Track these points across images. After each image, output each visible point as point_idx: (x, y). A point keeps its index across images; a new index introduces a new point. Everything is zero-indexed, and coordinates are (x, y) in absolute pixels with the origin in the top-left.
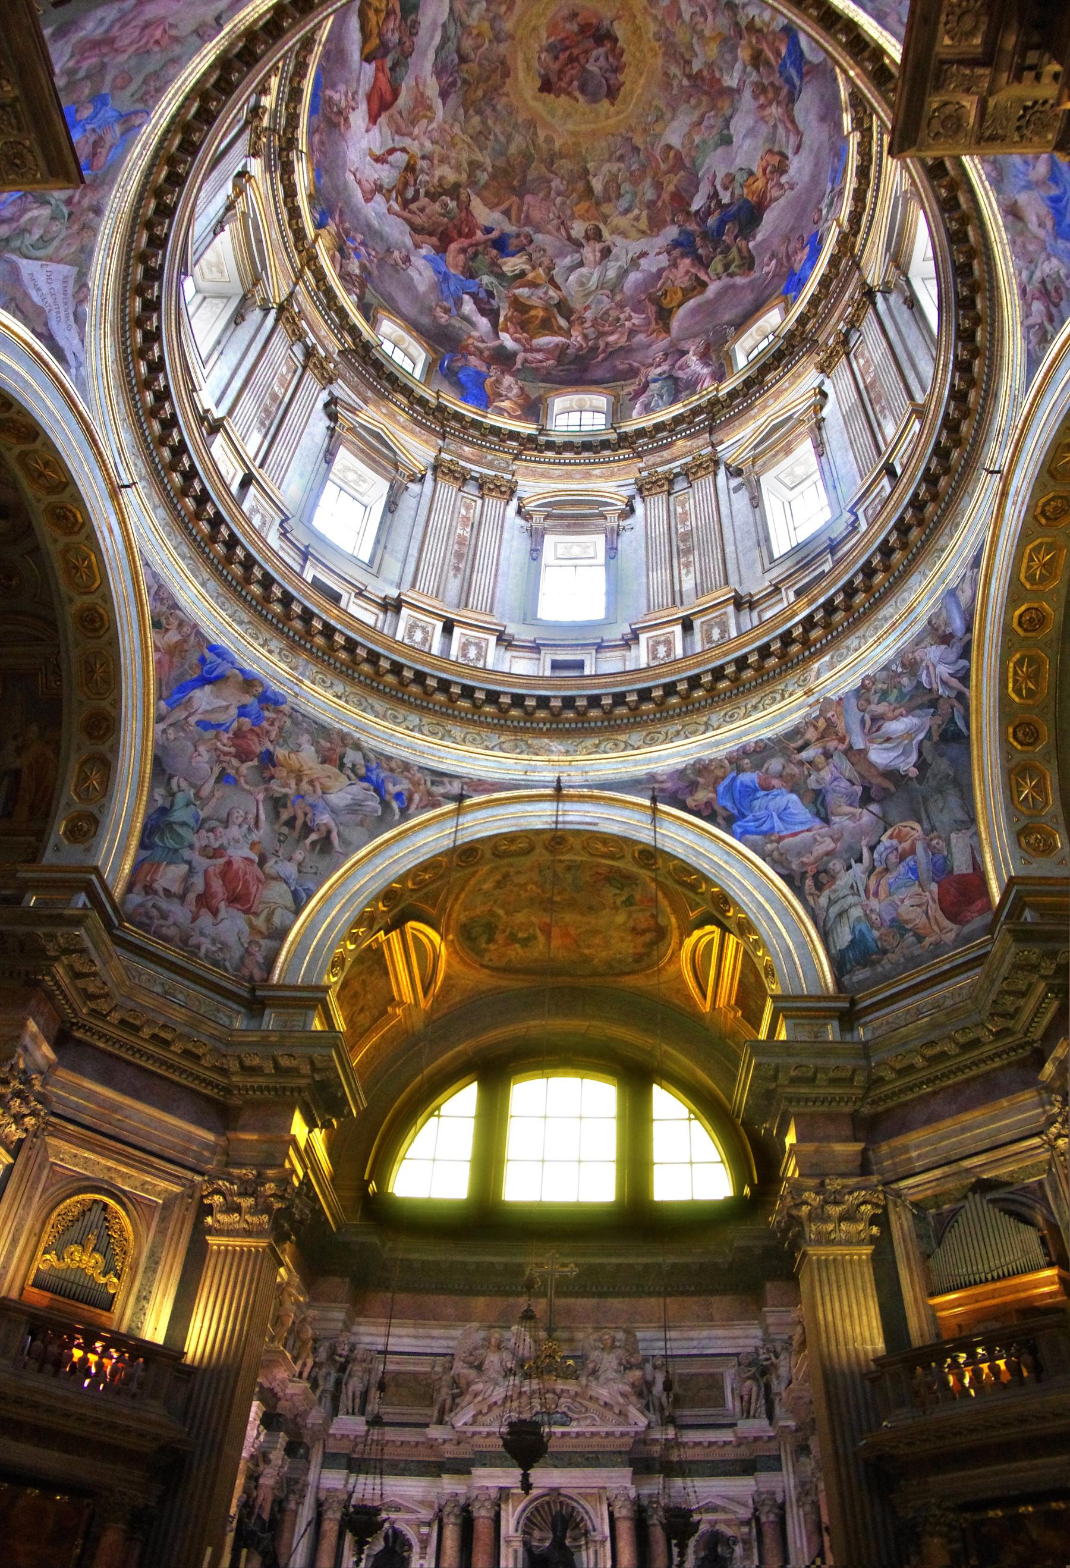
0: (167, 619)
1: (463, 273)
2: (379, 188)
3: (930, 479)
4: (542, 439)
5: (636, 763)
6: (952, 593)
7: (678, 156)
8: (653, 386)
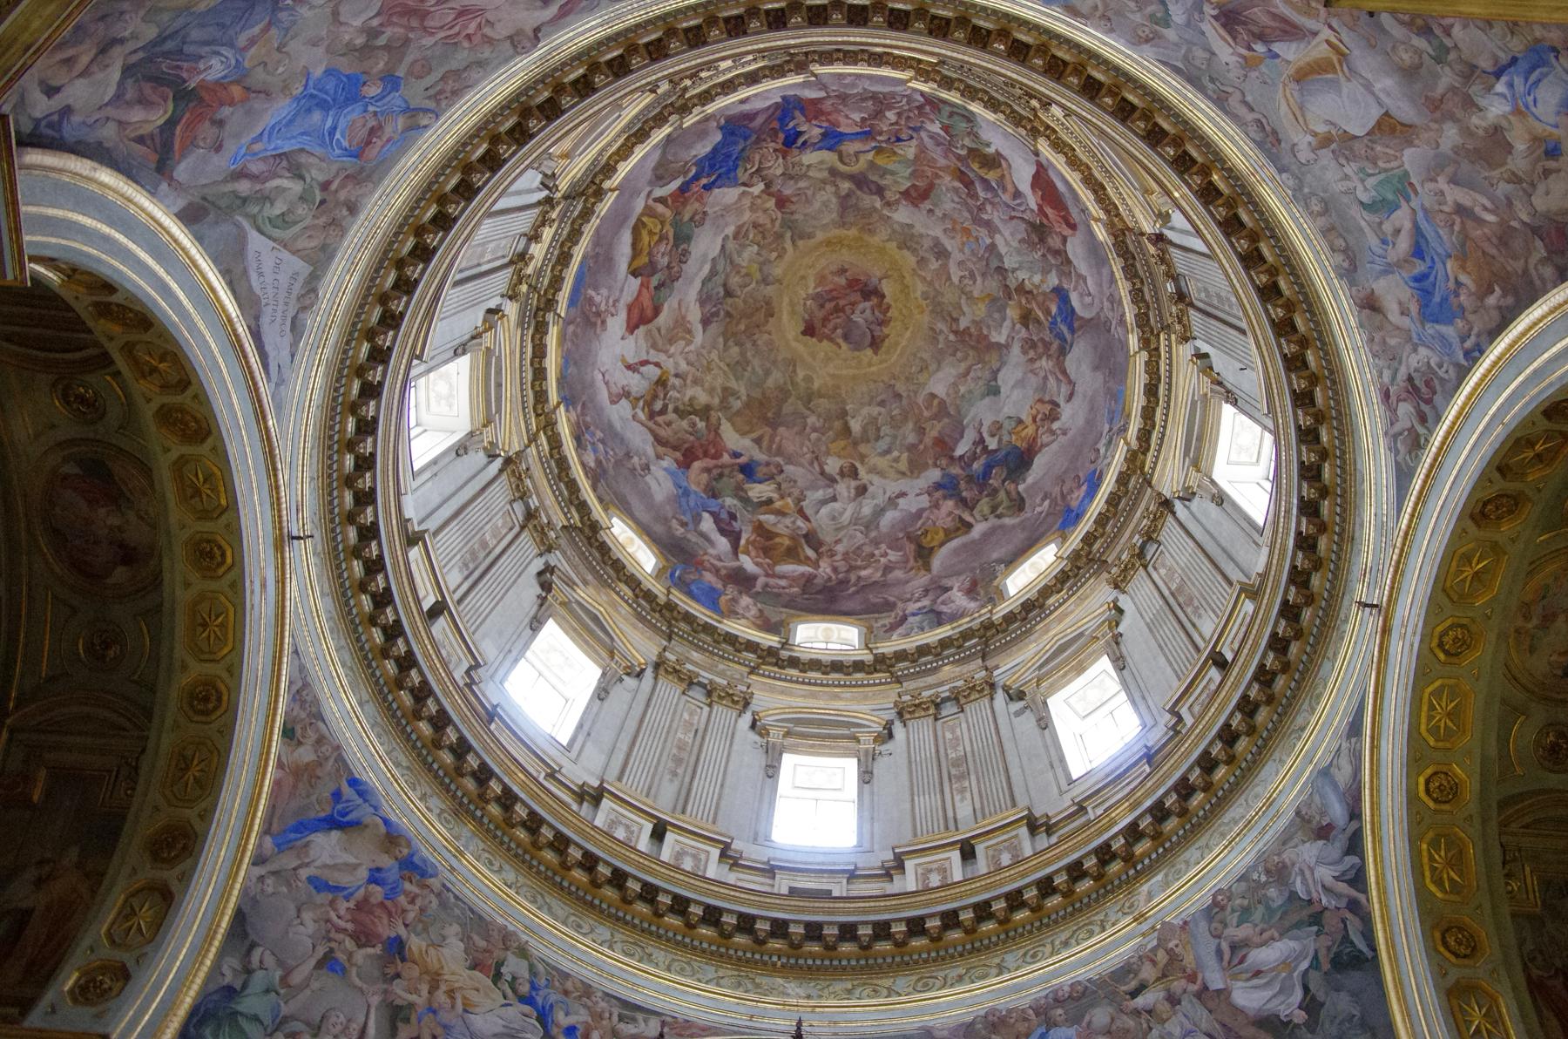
0: (304, 729)
1: (705, 491)
2: (626, 394)
3: (1264, 677)
4: (785, 654)
5: (906, 1014)
6: (1325, 773)
7: (942, 403)
8: (911, 619)
